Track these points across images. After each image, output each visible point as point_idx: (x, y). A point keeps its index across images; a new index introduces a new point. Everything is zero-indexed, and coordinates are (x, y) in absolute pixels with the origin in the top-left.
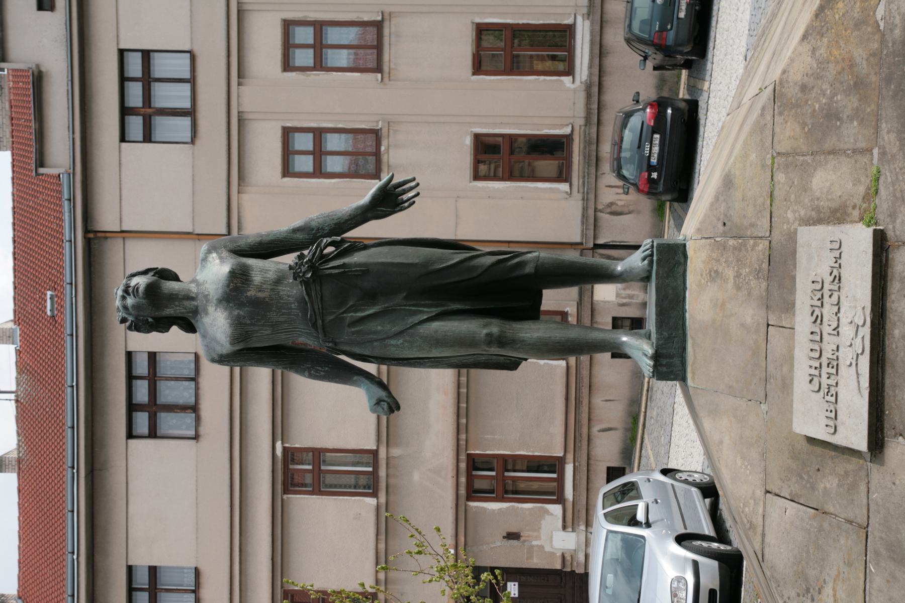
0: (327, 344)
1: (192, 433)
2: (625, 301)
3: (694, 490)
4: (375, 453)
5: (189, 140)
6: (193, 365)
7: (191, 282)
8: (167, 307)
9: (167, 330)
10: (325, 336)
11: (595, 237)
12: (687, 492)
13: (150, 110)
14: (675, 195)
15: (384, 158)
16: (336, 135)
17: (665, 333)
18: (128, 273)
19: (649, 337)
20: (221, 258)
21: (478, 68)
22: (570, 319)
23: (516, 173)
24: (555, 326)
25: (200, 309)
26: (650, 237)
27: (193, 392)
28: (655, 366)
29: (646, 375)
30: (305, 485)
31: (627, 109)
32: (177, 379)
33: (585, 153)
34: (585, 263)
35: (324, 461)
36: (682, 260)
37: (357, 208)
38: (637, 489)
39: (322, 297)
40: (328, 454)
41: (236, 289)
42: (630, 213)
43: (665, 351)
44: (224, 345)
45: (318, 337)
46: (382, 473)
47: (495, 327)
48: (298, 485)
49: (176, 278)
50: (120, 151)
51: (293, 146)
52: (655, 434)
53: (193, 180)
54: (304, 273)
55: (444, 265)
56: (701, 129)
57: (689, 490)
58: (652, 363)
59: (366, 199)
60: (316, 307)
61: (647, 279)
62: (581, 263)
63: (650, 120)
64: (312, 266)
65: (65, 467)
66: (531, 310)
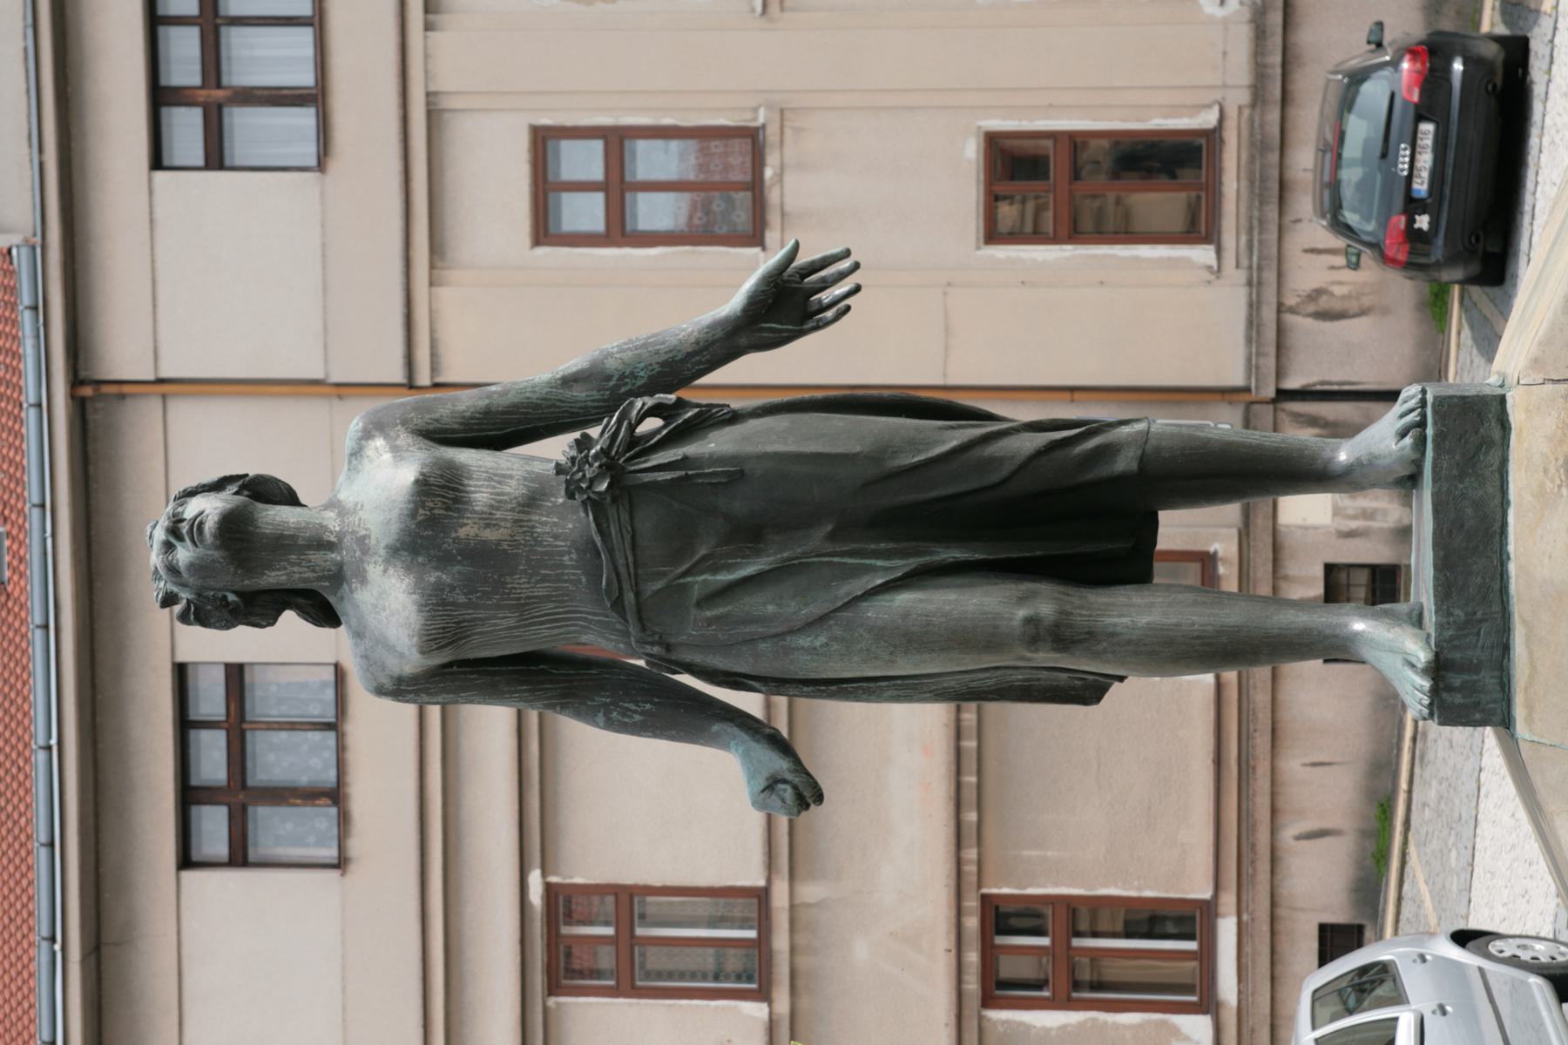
0: (648, 649)
1: (330, 853)
2: (1354, 524)
3: (1535, 981)
4: (762, 896)
5: (313, 162)
6: (330, 694)
7: (327, 507)
8: (270, 567)
9: (272, 621)
10: (644, 629)
11: (1280, 373)
12: (1517, 988)
13: (219, 94)
14: (1475, 268)
15: (773, 196)
16: (659, 143)
17: (1457, 612)
18: (177, 487)
19: (1418, 622)
20: (395, 449)
21: (993, 234)
22: (1221, 570)
23: (1087, 223)
24: (1190, 597)
25: (348, 572)
26: (1418, 381)
27: (330, 755)
28: (1435, 692)
29: (1408, 700)
30: (596, 973)
31: (1354, 63)
32: (292, 726)
33: (1251, 173)
34: (1260, 447)
35: (642, 916)
36: (1497, 434)
37: (713, 326)
38: (1396, 979)
39: (633, 538)
40: (650, 899)
41: (432, 522)
42: (1363, 312)
43: (1457, 655)
44: (408, 656)
45: (626, 634)
46: (781, 942)
47: (1044, 602)
48: (581, 974)
49: (291, 498)
50: (151, 192)
51: (557, 174)
52: (1435, 845)
53: (324, 256)
54: (592, 481)
55: (922, 457)
56: (1537, 107)
57: (1525, 984)
58: (1426, 684)
59: (733, 303)
60: (621, 561)
61: (1411, 481)
62: (1250, 446)
63: (1410, 90)
64: (610, 465)
65: (34, 937)
66: (1132, 561)
